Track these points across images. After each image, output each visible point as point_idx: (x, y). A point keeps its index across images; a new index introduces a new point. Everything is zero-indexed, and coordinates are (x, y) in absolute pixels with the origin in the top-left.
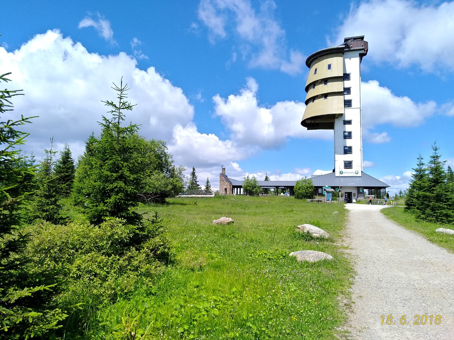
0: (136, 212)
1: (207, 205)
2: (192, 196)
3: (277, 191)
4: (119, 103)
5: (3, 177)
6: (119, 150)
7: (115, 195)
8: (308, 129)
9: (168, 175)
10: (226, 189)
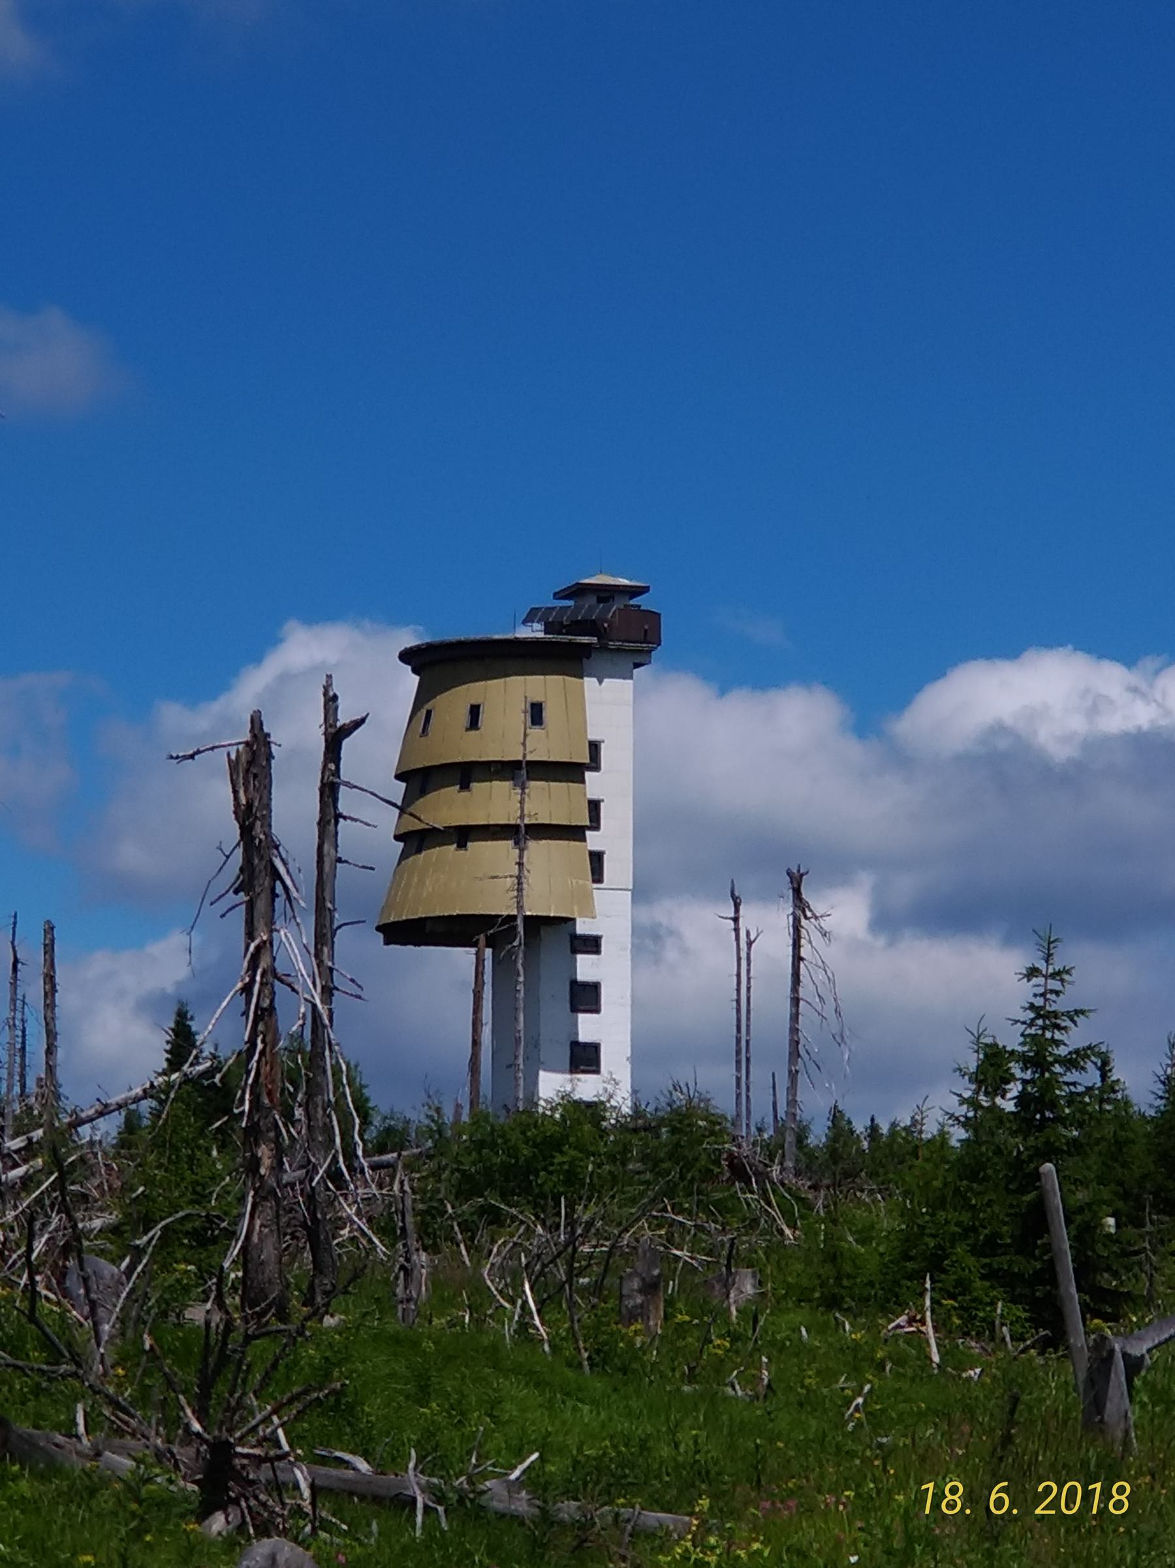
2: (1058, 1190)
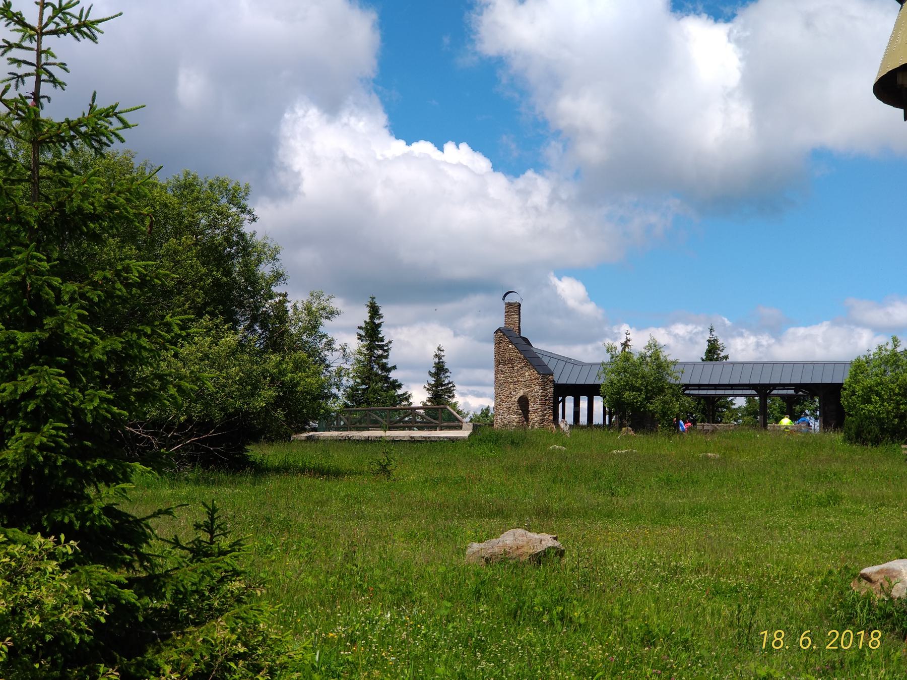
0: (124, 507)
1: (437, 473)
2: (365, 434)
3: (764, 405)
4: (38, 7)
5: (118, 212)
6: (41, 224)
7: (23, 430)
9: (257, 338)
10: (523, 403)
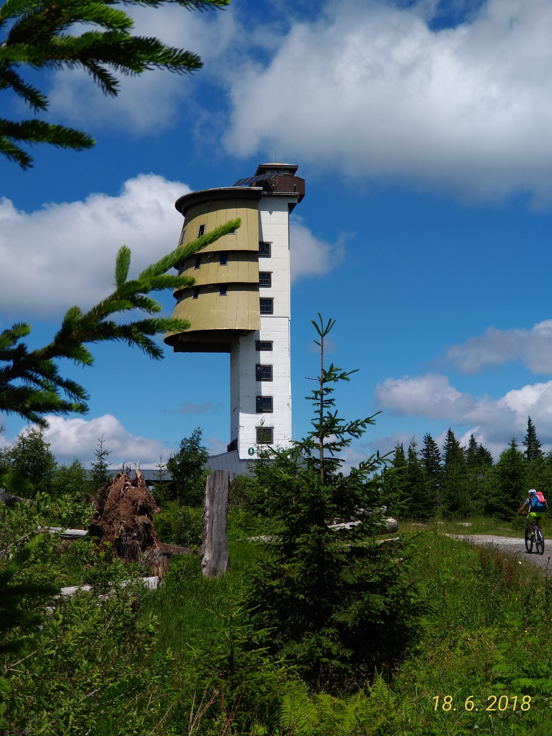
8: (175, 351)
